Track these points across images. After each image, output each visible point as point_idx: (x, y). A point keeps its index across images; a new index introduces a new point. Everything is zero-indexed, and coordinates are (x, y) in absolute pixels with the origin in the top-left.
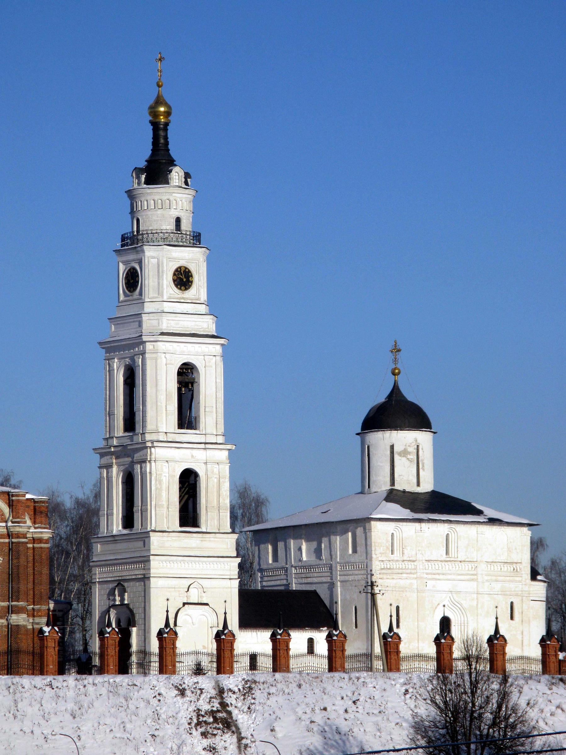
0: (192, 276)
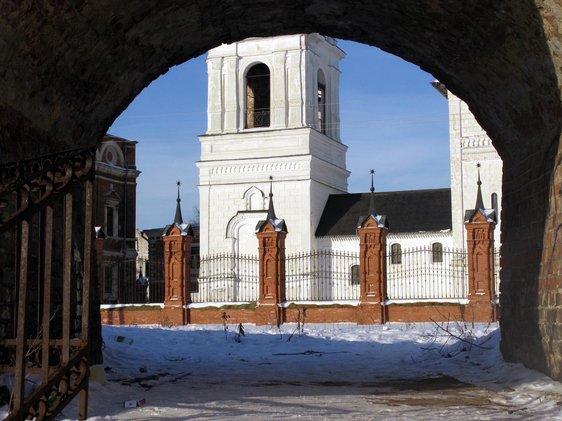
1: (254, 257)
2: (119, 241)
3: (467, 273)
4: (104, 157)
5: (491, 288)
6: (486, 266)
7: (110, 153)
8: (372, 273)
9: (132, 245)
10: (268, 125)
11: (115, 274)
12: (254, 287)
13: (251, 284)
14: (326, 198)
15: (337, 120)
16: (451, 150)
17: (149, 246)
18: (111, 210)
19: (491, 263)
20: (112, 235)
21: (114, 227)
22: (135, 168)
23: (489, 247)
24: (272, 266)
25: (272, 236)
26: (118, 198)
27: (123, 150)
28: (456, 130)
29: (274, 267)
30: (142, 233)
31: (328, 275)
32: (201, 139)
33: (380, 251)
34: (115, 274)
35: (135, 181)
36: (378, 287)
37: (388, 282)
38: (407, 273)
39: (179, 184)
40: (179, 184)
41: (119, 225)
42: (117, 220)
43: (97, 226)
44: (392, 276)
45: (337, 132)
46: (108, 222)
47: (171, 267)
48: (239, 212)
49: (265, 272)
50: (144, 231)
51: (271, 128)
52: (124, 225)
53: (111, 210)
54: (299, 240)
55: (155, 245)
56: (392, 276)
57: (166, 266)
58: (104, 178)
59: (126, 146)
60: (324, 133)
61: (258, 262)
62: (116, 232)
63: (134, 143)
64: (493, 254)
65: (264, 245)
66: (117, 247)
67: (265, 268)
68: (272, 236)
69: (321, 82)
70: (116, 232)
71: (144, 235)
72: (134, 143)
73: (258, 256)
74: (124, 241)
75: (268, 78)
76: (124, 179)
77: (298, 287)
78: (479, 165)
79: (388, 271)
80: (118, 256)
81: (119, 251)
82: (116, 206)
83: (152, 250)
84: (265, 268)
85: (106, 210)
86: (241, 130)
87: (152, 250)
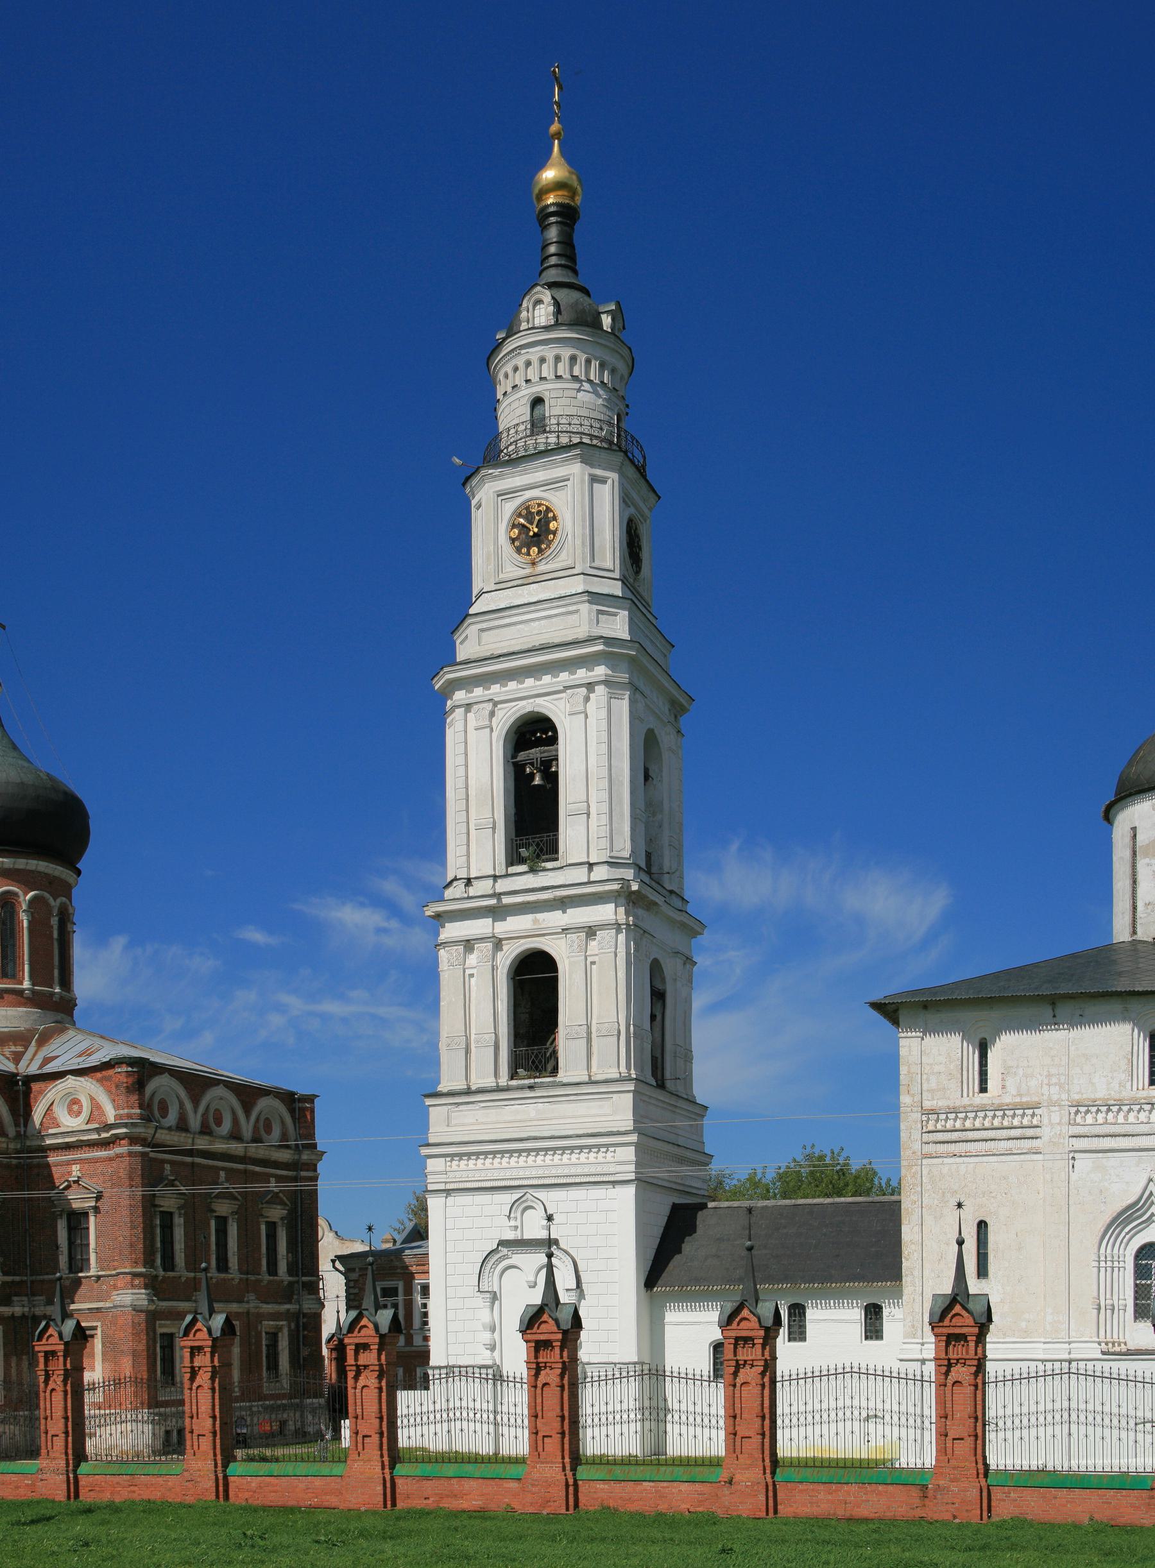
0: (555, 518)
1: (518, 1375)
2: (291, 1284)
3: (934, 1420)
4: (256, 1128)
5: (979, 1451)
6: (969, 1409)
7: (267, 1119)
8: (747, 1360)
9: (313, 1287)
10: (555, 1071)
11: (284, 1344)
12: (519, 1434)
13: (706, 1430)
14: (666, 1211)
15: (688, 1057)
16: (902, 1134)
17: (346, 1284)
18: (272, 1227)
19: (979, 1402)
20: (276, 1274)
21: (279, 1257)
22: (314, 1146)
23: (976, 1374)
24: (552, 1398)
25: (553, 1333)
26: (286, 1204)
27: (292, 1111)
28: (913, 1096)
29: (556, 1401)
30: (333, 1261)
31: (662, 1415)
32: (429, 1102)
33: (763, 1374)
34: (284, 1344)
35: (315, 1170)
36: (760, 1444)
37: (779, 1432)
38: (817, 1417)
39: (370, 1229)
40: (370, 1229)
41: (288, 1253)
42: (285, 1244)
43: (525, 770)
44: (787, 1421)
45: (688, 1080)
46: (267, 1249)
47: (358, 1394)
48: (502, 1243)
49: (539, 1408)
50: (339, 1257)
51: (557, 1079)
52: (297, 1251)
53: (272, 1227)
54: (609, 1332)
55: (356, 1281)
56: (787, 1421)
57: (350, 1391)
58: (257, 1169)
59: (298, 1105)
60: (661, 1085)
61: (525, 1386)
62: (282, 1267)
63: (311, 1099)
64: (984, 1383)
65: (539, 1346)
66: (287, 1294)
67: (539, 1400)
68: (553, 1333)
69: (659, 986)
70: (282, 1267)
71: (337, 1264)
72: (311, 1099)
73: (525, 1375)
74: (297, 1282)
75: (555, 981)
76: (294, 1166)
77: (431, 1435)
78: (960, 1205)
79: (779, 1411)
80: (288, 1310)
81: (290, 1302)
82: (282, 1219)
83: (352, 1291)
84: (539, 1400)
85: (263, 1227)
86: (504, 1080)
87: (352, 1291)
